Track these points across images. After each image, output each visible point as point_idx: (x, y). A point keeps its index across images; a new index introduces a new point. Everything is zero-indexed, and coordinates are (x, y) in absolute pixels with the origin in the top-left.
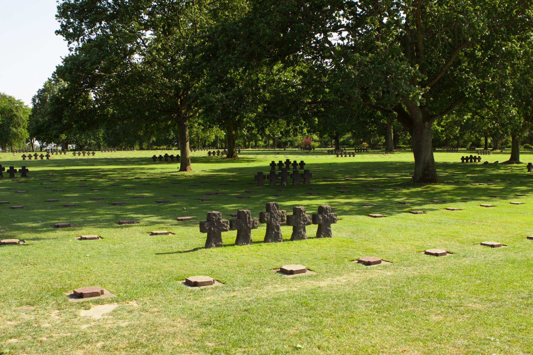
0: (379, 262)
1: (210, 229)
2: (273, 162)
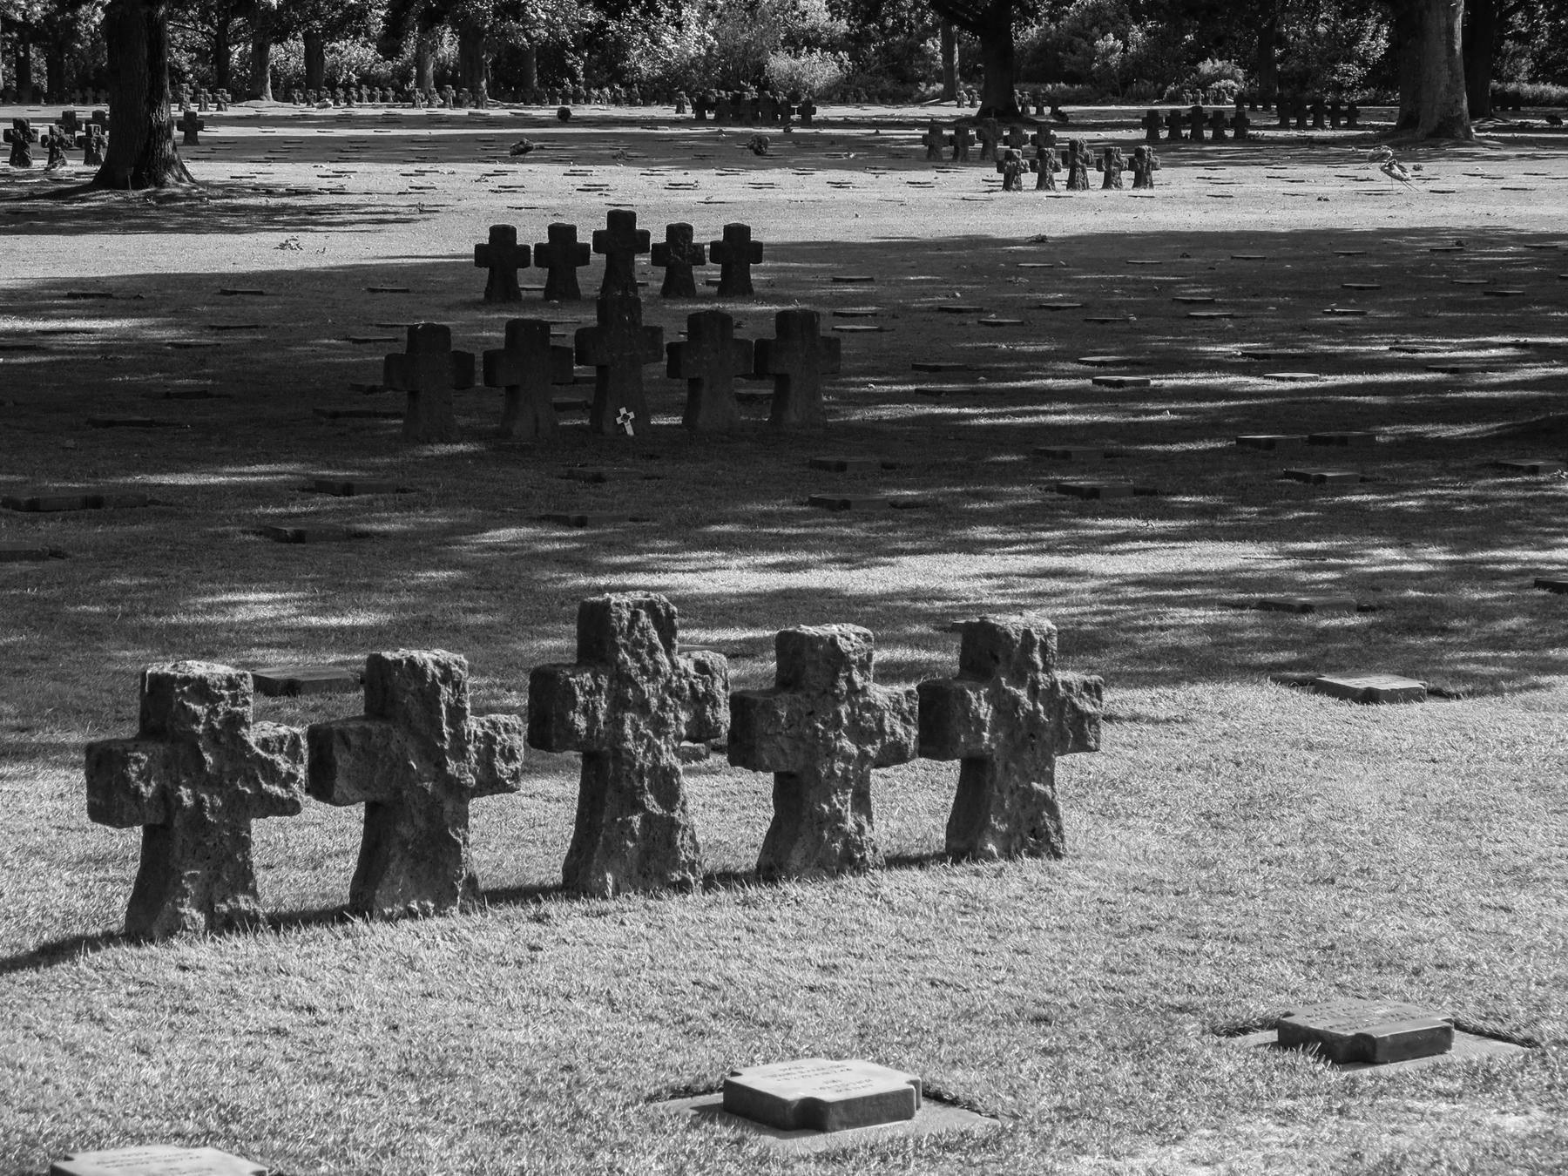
0: (1433, 1042)
1: (166, 796)
2: (503, 235)
